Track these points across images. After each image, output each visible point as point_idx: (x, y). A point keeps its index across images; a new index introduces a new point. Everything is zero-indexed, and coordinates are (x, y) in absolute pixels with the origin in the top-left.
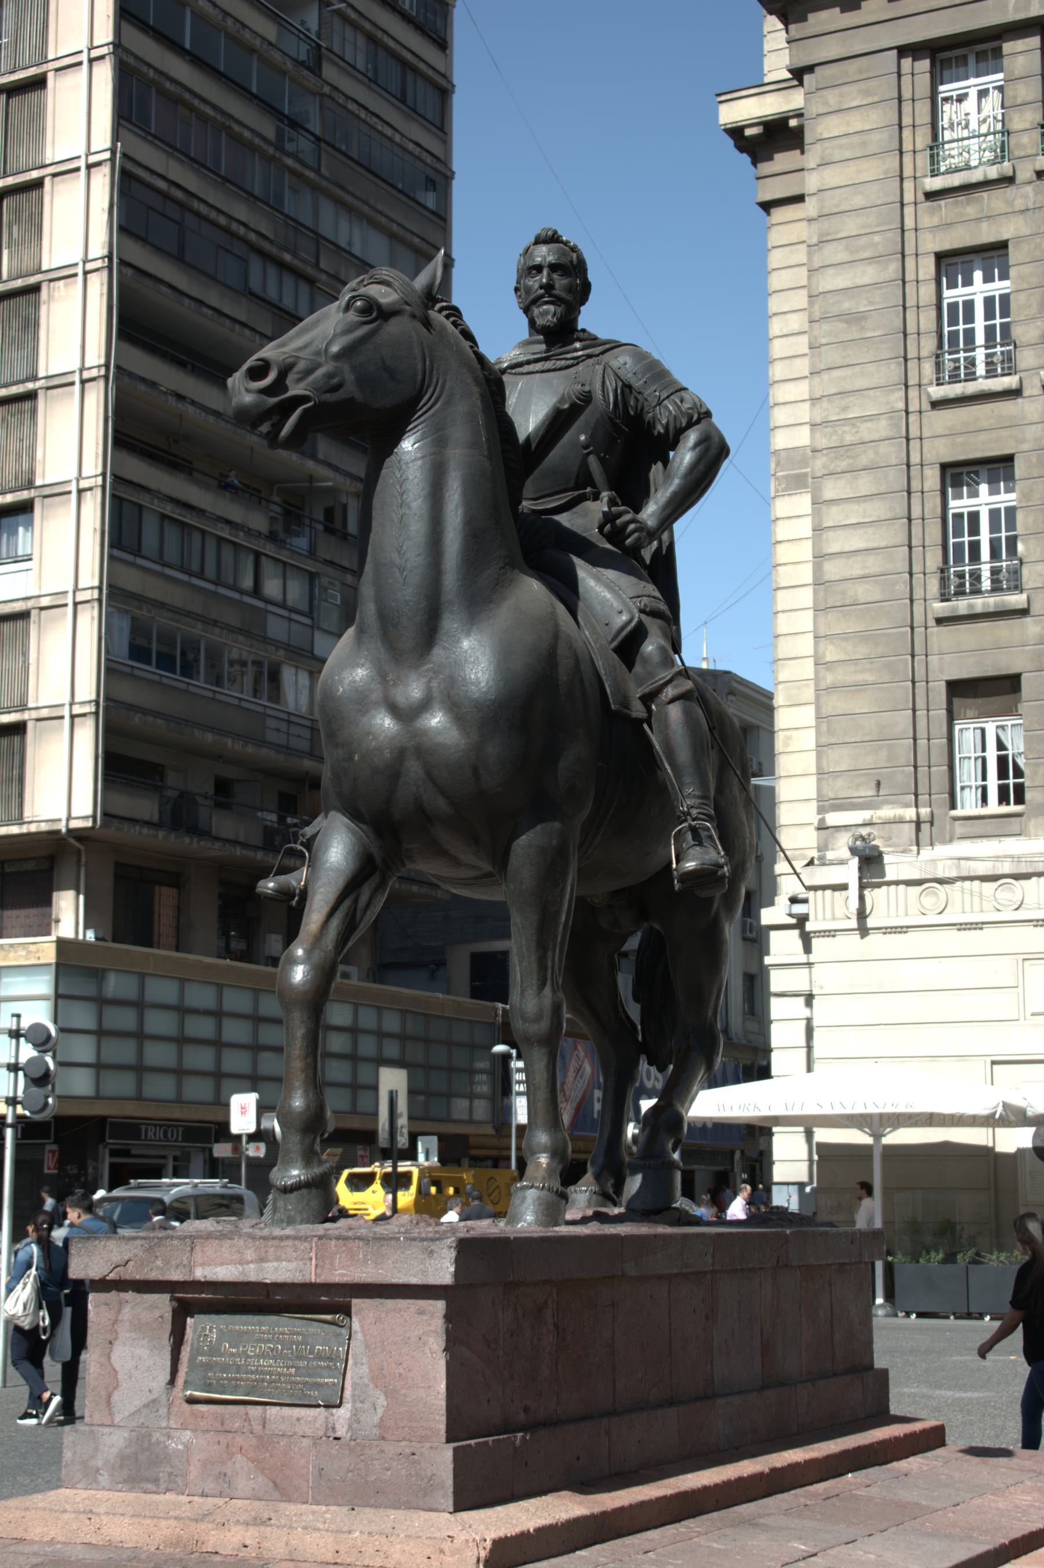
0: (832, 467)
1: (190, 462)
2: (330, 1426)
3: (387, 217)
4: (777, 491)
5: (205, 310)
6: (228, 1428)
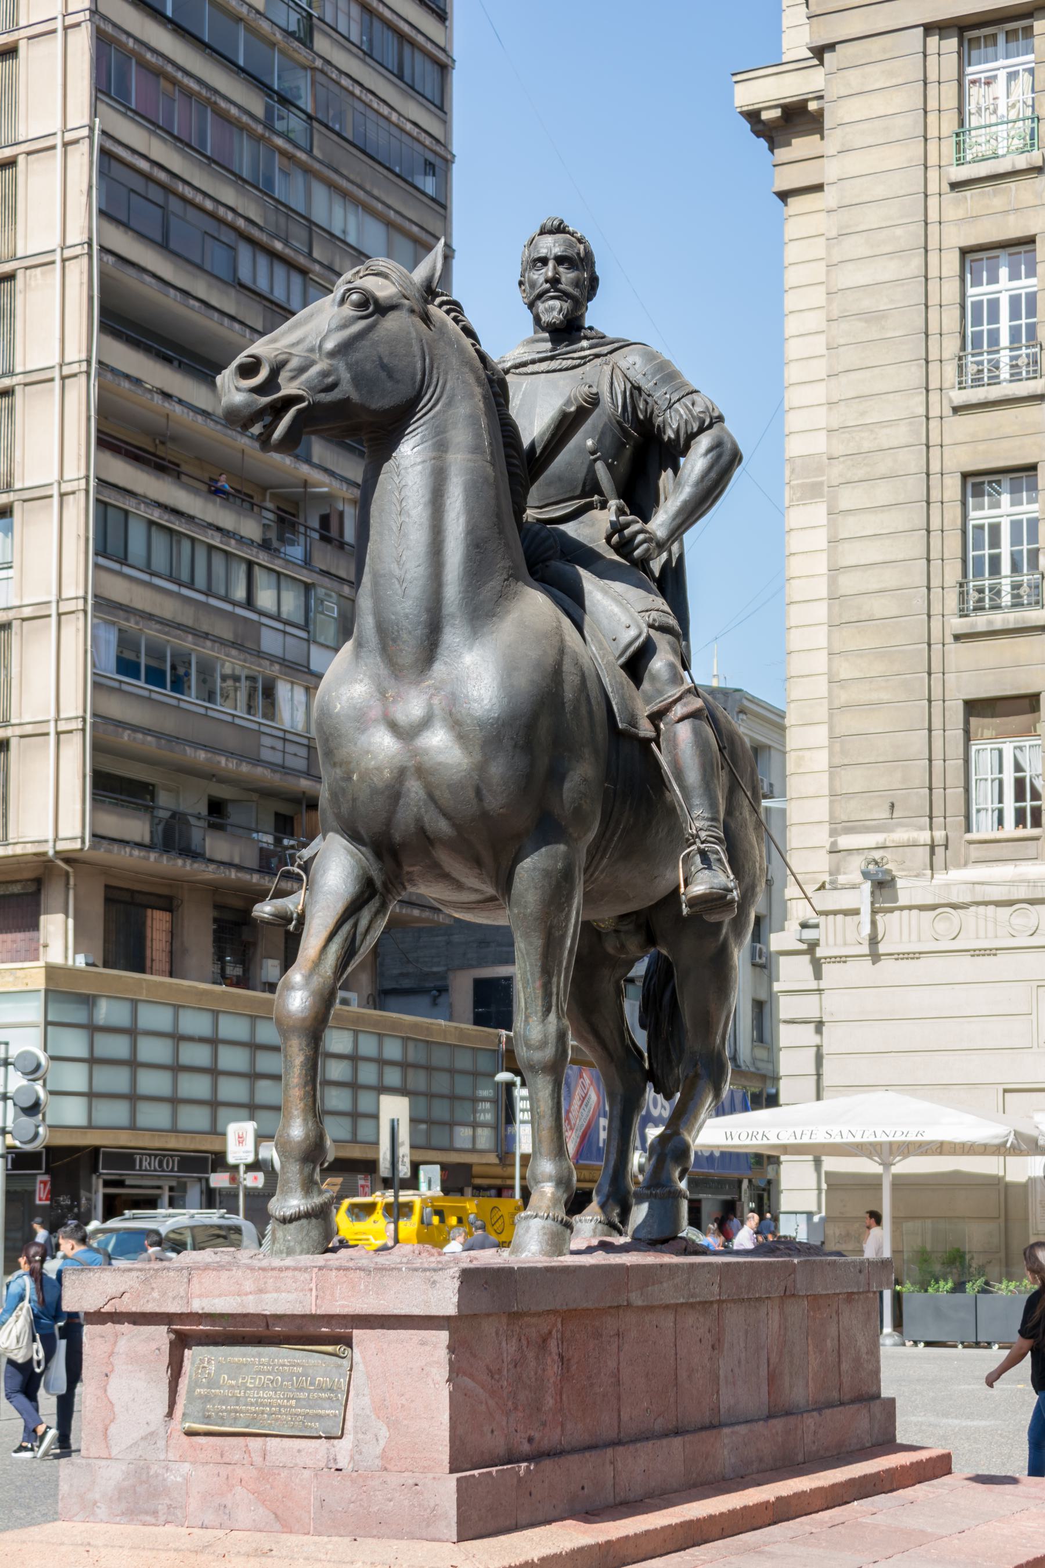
1: (178, 465)
2: (331, 1457)
3: (384, 203)
4: (792, 500)
5: (192, 302)
6: (227, 1461)
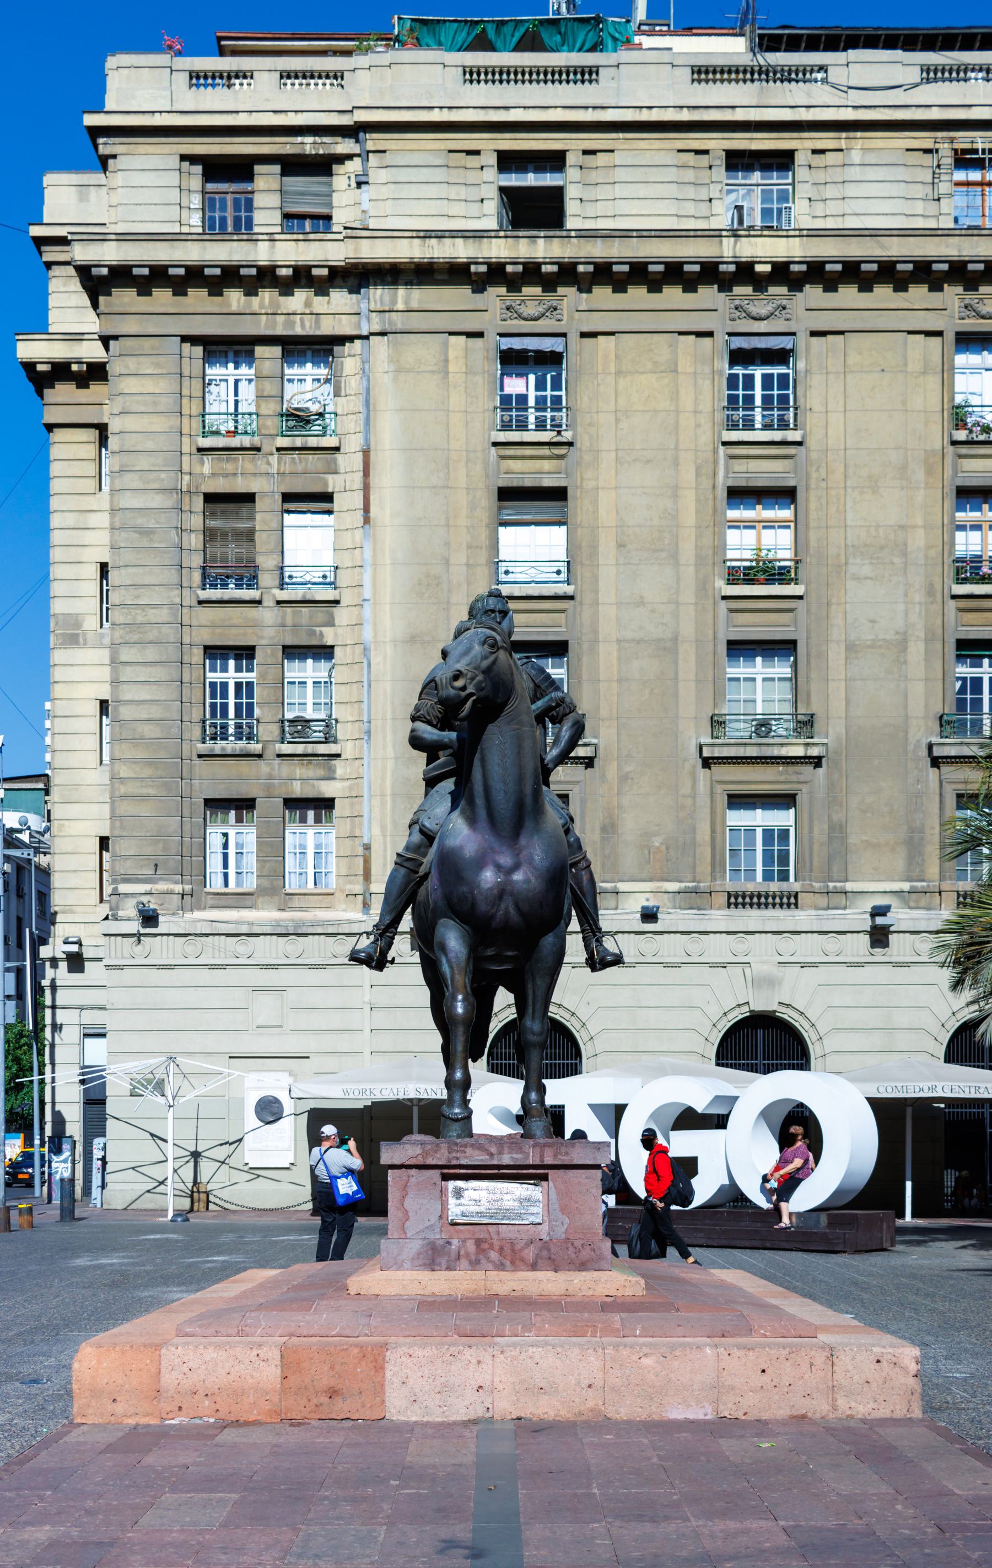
0: (127, 638)
4: (55, 644)
